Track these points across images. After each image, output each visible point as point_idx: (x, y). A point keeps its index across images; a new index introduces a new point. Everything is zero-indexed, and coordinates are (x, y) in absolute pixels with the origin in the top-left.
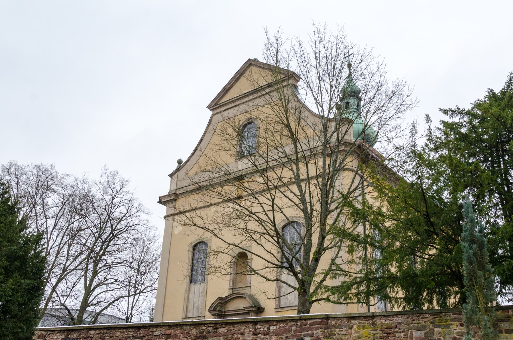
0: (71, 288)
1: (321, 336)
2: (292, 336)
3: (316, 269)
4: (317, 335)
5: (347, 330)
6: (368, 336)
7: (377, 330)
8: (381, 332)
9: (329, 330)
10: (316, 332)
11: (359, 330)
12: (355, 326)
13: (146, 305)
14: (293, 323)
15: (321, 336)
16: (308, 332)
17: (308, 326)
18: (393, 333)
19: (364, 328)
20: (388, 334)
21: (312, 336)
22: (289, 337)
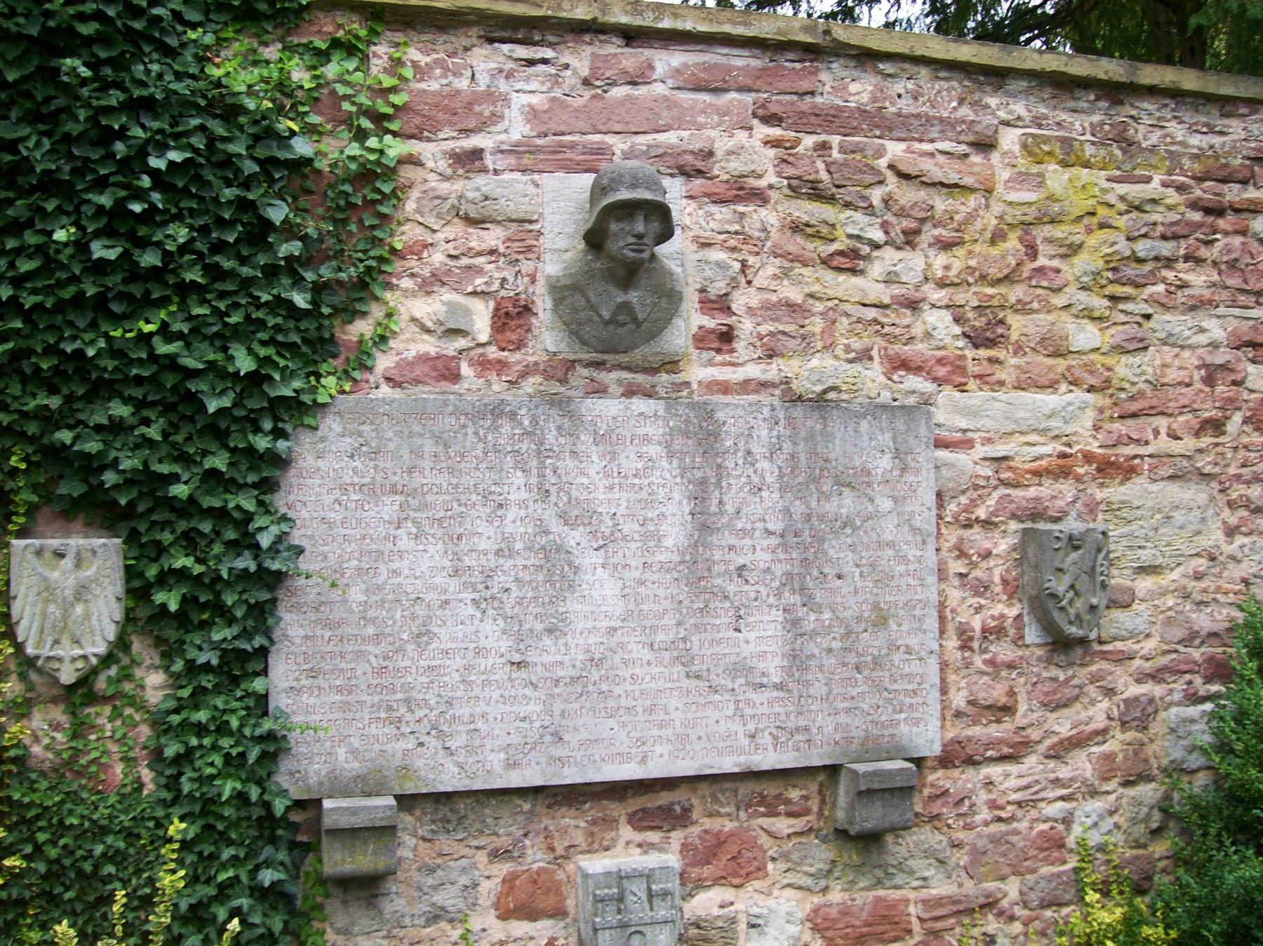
0: (602, 551)
1: (771, 178)
2: (514, 150)
3: (825, 766)
4: (736, 166)
5: (966, 155)
6: (1102, 211)
7: (1148, 180)
8: (1173, 197)
9: (835, 140)
10: (730, 144)
11: (1035, 169)
12: (1009, 139)
13: (1200, 783)
14: (522, 52)
15: (771, 178)
16: (662, 137)
17: (659, 89)
18: (1237, 211)
19: (1070, 157)
20: (1208, 211)
21: (700, 173)
22: (489, 161)
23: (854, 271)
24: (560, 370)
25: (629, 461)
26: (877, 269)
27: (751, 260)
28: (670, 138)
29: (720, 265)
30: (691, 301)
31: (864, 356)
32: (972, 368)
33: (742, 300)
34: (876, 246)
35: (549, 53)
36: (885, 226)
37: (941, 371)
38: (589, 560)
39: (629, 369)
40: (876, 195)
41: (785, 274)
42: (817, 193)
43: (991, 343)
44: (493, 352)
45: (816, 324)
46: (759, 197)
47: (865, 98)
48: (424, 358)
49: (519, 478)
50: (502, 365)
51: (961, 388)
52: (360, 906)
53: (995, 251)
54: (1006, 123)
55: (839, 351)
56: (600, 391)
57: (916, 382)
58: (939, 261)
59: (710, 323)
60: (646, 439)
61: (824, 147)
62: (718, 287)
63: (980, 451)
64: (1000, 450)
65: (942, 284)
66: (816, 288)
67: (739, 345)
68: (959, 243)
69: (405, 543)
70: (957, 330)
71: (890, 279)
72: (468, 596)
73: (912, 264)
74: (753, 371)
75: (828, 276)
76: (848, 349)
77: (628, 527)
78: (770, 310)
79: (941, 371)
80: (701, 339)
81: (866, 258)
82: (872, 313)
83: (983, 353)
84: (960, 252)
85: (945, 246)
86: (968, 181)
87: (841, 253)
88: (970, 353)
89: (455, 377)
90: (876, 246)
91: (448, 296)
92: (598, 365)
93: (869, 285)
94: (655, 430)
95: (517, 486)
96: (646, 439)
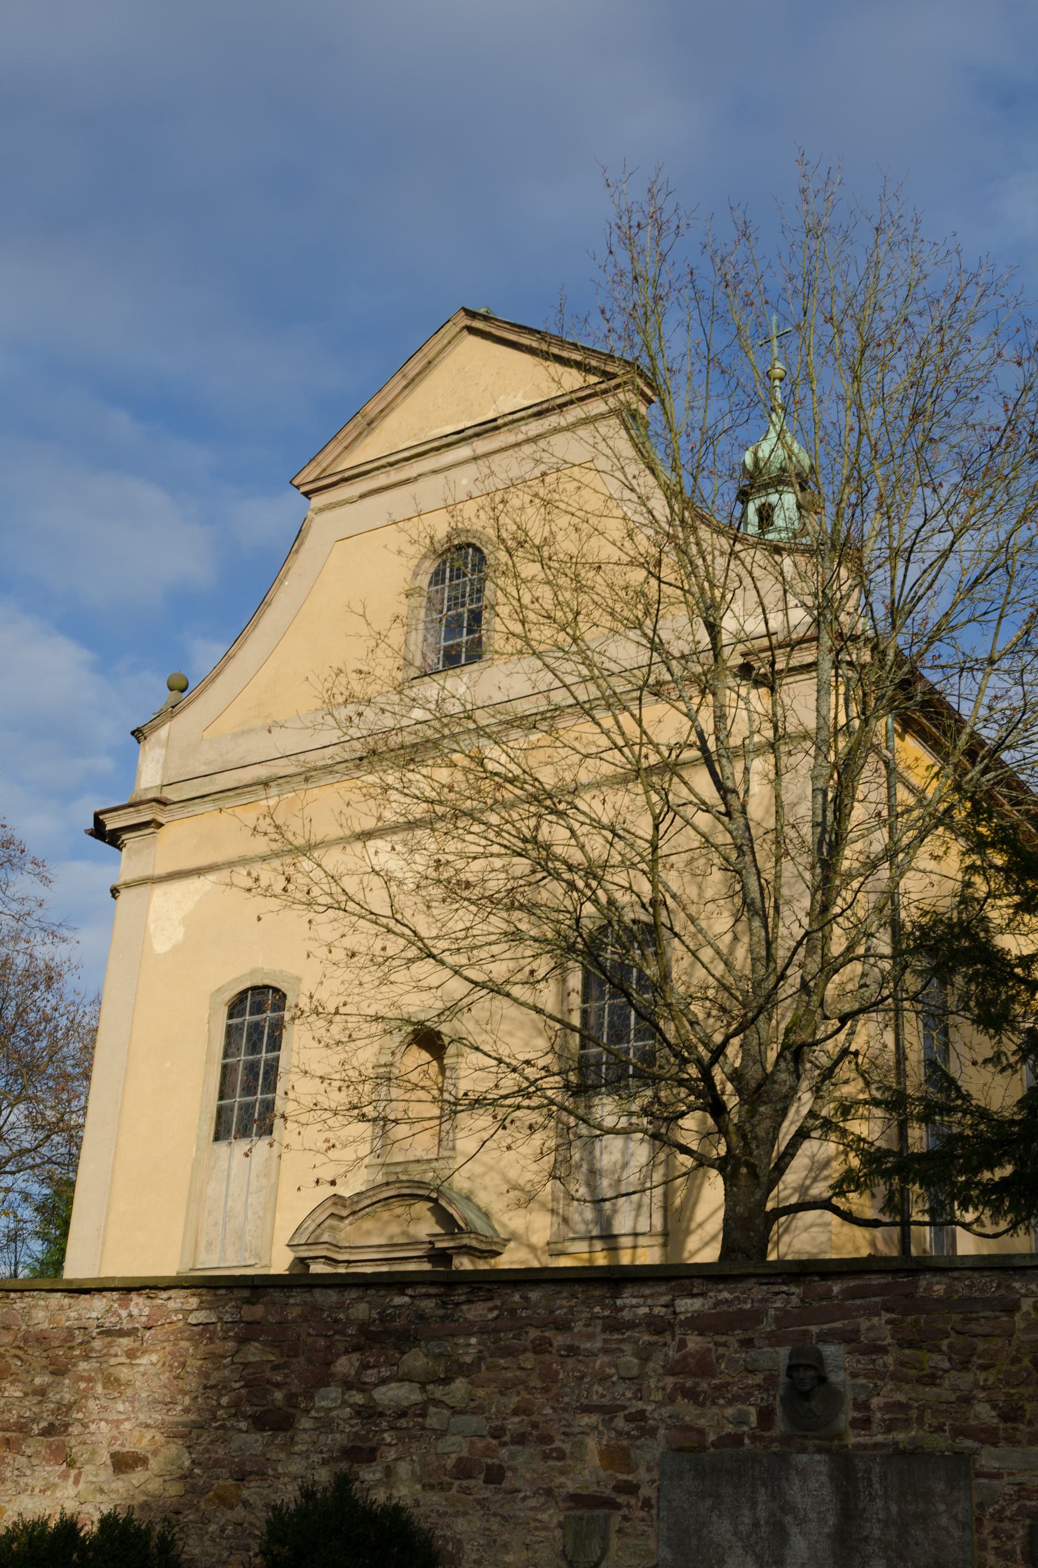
1: (889, 1340)
2: (770, 1336)
15: (889, 1340)
22: (757, 1343)
23: (933, 1384)
24: (786, 1440)
25: (813, 1484)
26: (947, 1383)
27: (879, 1383)
28: (838, 1324)
29: (863, 1386)
30: (849, 1404)
31: (940, 1428)
32: (1001, 1433)
33: (875, 1402)
34: (946, 1371)
35: (785, 1288)
36: (950, 1360)
37: (983, 1436)
38: (794, 1530)
39: (819, 1438)
40: (944, 1345)
41: (898, 1389)
42: (911, 1345)
43: (1014, 1420)
44: (758, 1432)
45: (914, 1413)
46: (884, 1350)
47: (942, 1292)
48: (729, 1435)
49: (763, 1490)
50: (761, 1438)
51: (995, 1445)
52: (145, 1506)
53: (1014, 1369)
54: (1023, 1296)
55: (926, 1427)
56: (803, 1450)
57: (969, 1443)
58: (982, 1376)
59: (857, 1415)
60: (820, 1473)
61: (916, 1321)
62: (862, 1397)
63: (1006, 1479)
64: (1019, 1479)
65: (983, 1388)
66: (913, 1395)
67: (874, 1426)
68: (993, 1366)
69: (714, 1518)
70: (994, 1413)
71: (954, 1389)
72: (740, 1544)
73: (965, 1380)
74: (880, 1438)
75: (920, 1388)
76: (930, 1426)
77: (812, 1515)
78: (889, 1407)
79: (983, 1436)
80: (854, 1424)
81: (941, 1377)
82: (944, 1407)
83: (1009, 1425)
84: (993, 1371)
85: (984, 1368)
86: (997, 1332)
87: (926, 1376)
88: (1001, 1426)
89: (742, 1444)
90: (946, 1371)
91: (740, 1406)
92: (805, 1437)
93: (944, 1392)
94: (823, 1468)
95: (762, 1495)
96: (820, 1473)
